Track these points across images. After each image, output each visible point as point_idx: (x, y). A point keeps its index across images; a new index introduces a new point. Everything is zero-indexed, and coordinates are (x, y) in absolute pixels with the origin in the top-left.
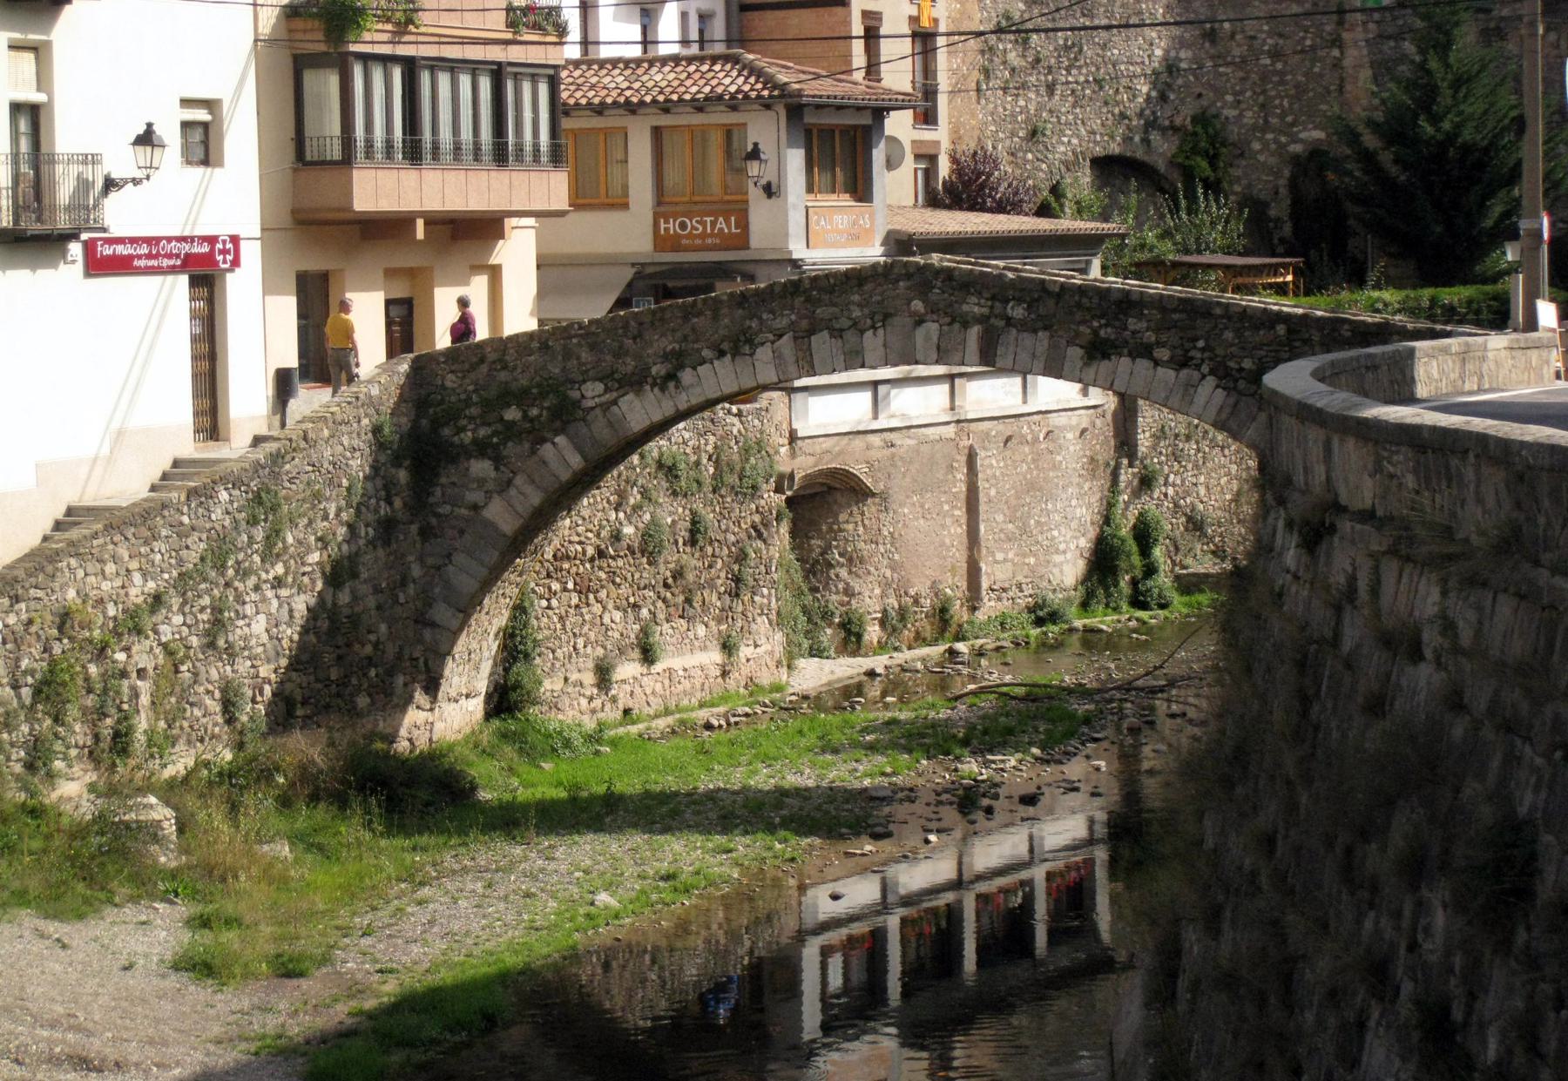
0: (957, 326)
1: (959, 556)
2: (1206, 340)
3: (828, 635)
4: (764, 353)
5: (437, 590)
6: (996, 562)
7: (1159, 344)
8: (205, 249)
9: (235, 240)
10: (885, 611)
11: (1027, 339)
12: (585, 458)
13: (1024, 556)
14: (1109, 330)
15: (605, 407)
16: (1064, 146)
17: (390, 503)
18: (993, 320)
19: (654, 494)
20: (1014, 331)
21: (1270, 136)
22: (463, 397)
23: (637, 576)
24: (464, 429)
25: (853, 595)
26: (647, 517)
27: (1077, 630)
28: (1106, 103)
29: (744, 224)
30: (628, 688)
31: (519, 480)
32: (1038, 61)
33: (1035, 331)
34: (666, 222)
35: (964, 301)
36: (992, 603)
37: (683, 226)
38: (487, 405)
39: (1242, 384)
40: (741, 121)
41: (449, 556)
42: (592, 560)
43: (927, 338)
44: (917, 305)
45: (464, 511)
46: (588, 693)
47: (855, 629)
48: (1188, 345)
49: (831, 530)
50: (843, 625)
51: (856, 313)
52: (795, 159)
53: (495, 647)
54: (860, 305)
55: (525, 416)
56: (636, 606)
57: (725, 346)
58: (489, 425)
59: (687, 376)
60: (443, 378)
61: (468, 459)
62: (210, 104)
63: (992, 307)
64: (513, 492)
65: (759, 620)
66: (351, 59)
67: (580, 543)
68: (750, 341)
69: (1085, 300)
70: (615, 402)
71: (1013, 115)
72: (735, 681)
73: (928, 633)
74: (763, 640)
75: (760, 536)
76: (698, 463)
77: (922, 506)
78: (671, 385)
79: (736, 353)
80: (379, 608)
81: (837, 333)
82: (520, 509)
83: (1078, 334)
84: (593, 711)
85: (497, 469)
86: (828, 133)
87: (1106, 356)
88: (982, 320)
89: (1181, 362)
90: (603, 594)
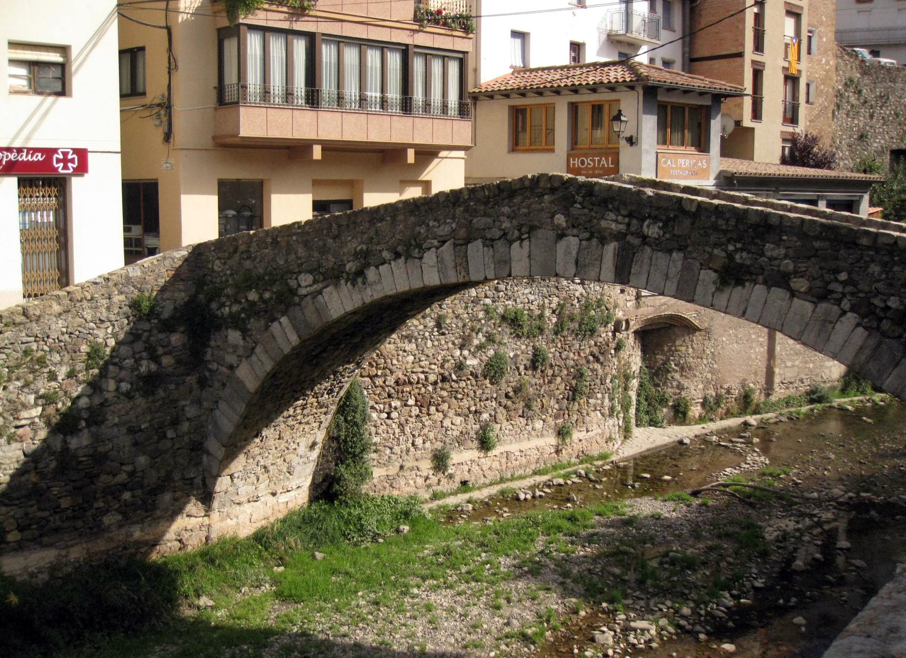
0: (594, 241)
1: (762, 366)
2: (849, 274)
4: (430, 258)
6: (787, 367)
7: (796, 273)
8: (39, 157)
9: (82, 154)
10: (705, 399)
11: (661, 259)
12: (299, 337)
13: (806, 362)
14: (744, 254)
16: (877, 143)
18: (629, 238)
19: (498, 338)
23: (479, 392)
25: (683, 389)
27: (834, 408)
28: (900, 124)
29: (616, 162)
30: (466, 468)
31: (258, 350)
32: (865, 102)
33: (670, 251)
34: (574, 160)
35: (603, 218)
36: (782, 391)
37: (583, 163)
40: (617, 98)
42: (435, 383)
43: (567, 252)
44: (560, 219)
45: (224, 369)
46: (425, 474)
47: (682, 409)
48: (827, 277)
49: (670, 350)
50: (674, 407)
51: (506, 224)
52: (649, 124)
55: (261, 298)
57: (400, 249)
59: (371, 273)
61: (227, 328)
62: (64, 50)
63: (628, 225)
64: (254, 358)
65: (592, 414)
66: (242, 27)
67: (423, 372)
68: (419, 246)
69: (721, 222)
70: (320, 292)
71: (851, 128)
73: (735, 410)
74: (595, 426)
75: (597, 360)
76: (541, 316)
77: (736, 336)
79: (409, 256)
81: (489, 243)
84: (429, 486)
85: (244, 339)
86: (679, 109)
87: (740, 282)
88: (619, 237)
89: (820, 295)
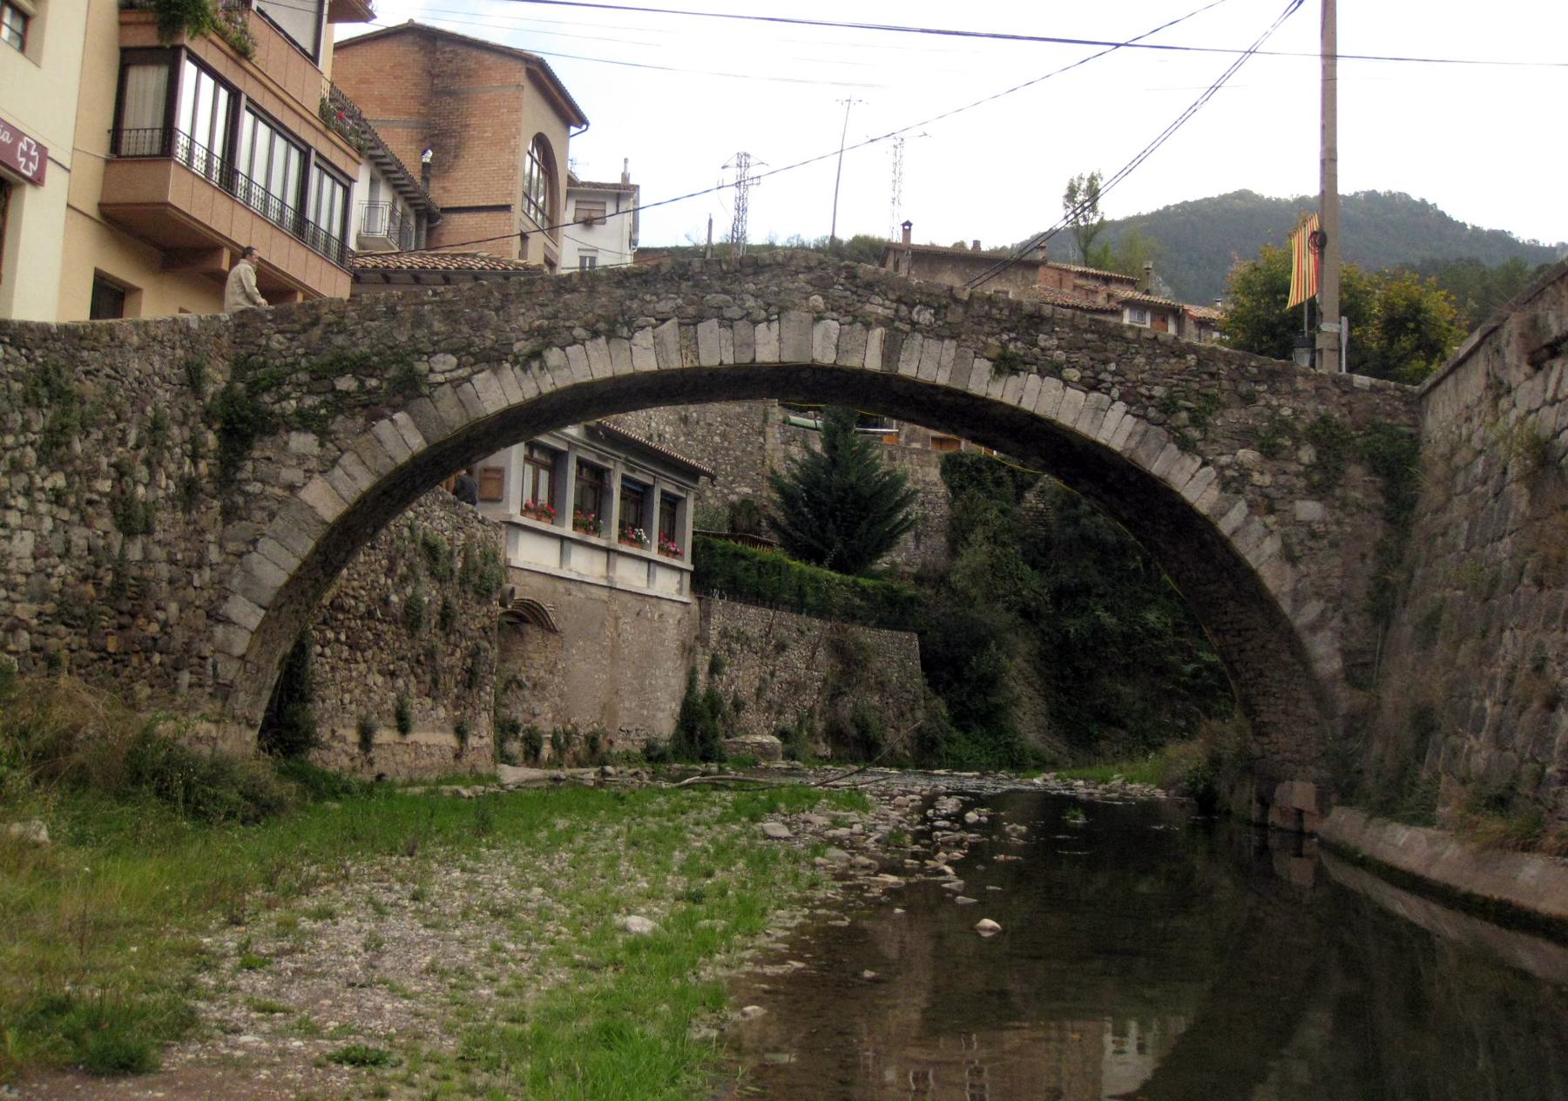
0: (858, 326)
3: (515, 747)
4: (644, 339)
5: (235, 582)
10: (555, 733)
11: (933, 346)
15: (456, 384)
17: (195, 463)
18: (897, 324)
20: (919, 336)
22: (290, 360)
24: (287, 397)
26: (409, 590)
31: (347, 459)
33: (941, 338)
39: (1152, 412)
41: (254, 542)
43: (826, 336)
44: (817, 300)
45: (278, 491)
48: (1099, 367)
54: (756, 296)
56: (393, 674)
57: (602, 326)
58: (318, 394)
59: (553, 356)
60: (269, 338)
61: (288, 432)
63: (897, 311)
64: (338, 472)
67: (354, 597)
70: (468, 379)
79: (611, 335)
80: (171, 582)
82: (345, 494)
83: (986, 346)
85: (321, 445)
87: (1015, 371)
88: (886, 322)
89: (1091, 385)
90: (369, 654)
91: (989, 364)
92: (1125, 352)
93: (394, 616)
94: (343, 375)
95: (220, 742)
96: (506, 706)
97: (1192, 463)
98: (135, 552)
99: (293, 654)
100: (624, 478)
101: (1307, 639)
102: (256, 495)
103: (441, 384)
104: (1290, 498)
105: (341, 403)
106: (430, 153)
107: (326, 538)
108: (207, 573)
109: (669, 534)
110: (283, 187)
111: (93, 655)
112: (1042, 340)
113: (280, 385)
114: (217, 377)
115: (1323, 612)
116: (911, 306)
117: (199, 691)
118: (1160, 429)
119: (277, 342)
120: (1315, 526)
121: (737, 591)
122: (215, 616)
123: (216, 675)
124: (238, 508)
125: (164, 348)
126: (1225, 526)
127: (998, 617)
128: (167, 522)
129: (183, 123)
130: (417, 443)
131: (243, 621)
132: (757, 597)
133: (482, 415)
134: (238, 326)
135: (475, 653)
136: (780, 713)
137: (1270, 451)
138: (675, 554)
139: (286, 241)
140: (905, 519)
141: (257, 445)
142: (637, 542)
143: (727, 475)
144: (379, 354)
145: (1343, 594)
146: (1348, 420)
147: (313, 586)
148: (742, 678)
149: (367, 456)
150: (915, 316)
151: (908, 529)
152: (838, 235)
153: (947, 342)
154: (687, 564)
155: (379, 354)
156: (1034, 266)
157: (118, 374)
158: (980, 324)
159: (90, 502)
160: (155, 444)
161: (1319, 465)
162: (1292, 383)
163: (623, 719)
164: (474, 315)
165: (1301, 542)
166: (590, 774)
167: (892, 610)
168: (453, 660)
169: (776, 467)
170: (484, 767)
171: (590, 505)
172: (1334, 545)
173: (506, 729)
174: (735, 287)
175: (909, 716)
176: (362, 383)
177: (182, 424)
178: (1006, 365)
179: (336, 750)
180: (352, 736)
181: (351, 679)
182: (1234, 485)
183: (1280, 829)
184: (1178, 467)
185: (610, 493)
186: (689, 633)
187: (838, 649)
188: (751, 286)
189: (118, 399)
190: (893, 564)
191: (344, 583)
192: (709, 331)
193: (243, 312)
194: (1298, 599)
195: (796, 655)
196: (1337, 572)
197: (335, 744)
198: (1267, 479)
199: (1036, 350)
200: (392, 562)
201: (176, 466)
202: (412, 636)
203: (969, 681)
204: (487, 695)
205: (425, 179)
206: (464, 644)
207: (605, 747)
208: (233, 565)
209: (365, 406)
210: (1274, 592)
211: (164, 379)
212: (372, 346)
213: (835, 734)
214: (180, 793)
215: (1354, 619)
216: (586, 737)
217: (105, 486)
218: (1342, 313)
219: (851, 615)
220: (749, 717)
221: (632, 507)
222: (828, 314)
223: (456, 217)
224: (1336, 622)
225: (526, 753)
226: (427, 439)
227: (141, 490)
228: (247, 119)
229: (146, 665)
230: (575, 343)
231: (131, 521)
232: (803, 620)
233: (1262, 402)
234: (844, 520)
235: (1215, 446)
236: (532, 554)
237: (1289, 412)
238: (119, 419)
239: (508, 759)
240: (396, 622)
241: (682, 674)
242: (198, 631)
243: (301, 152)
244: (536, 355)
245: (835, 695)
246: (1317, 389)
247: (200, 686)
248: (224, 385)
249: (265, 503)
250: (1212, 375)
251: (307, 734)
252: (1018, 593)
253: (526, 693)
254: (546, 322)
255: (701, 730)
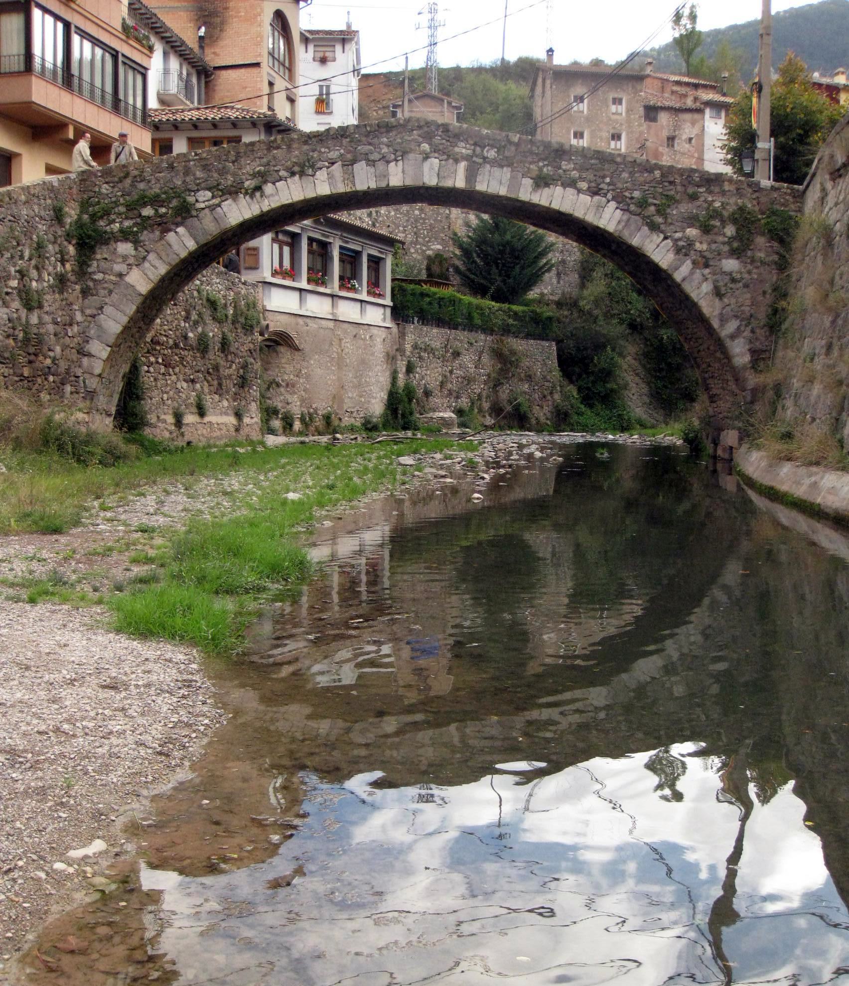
0: (451, 161)
3: (276, 424)
4: (322, 175)
5: (92, 332)
7: (582, 179)
10: (302, 414)
11: (497, 171)
14: (550, 168)
15: (212, 208)
17: (63, 265)
18: (474, 159)
20: (488, 166)
21: (418, 247)
22: (113, 199)
24: (114, 221)
31: (151, 257)
33: (502, 167)
35: (456, 146)
38: (130, 207)
43: (431, 168)
44: (426, 147)
45: (113, 278)
53: (121, 385)
54: (388, 146)
56: (193, 381)
57: (296, 169)
59: (268, 188)
60: (100, 187)
61: (116, 242)
63: (474, 151)
64: (147, 265)
70: (219, 205)
72: (242, 436)
78: (258, 194)
79: (302, 174)
81: (371, 163)
82: (152, 277)
85: (136, 249)
87: (547, 185)
88: (467, 158)
89: (595, 192)
90: (177, 370)
91: (532, 181)
92: (615, 171)
93: (191, 345)
94: (145, 207)
95: (91, 424)
96: (269, 398)
97: (657, 238)
98: (34, 320)
99: (130, 372)
100: (341, 247)
101: (728, 343)
102: (100, 281)
103: (203, 209)
104: (718, 258)
105: (145, 223)
106: (203, 29)
107: (144, 303)
108: (75, 328)
109: (375, 284)
110: (103, 80)
111: (17, 379)
112: (565, 165)
113: (109, 214)
114: (72, 213)
115: (738, 328)
116: (483, 147)
117: (77, 396)
118: (637, 218)
119: (105, 189)
120: (734, 275)
121: (425, 318)
122: (82, 353)
123: (85, 386)
124: (90, 289)
125: (39, 200)
126: (678, 276)
127: (614, 329)
128: (51, 301)
129: (37, 50)
130: (191, 245)
131: (98, 354)
132: (440, 322)
133: (228, 226)
134: (81, 180)
135: (245, 366)
136: (457, 397)
137: (706, 229)
138: (380, 296)
139: (107, 115)
140: (546, 264)
141: (98, 251)
142: (353, 289)
143: (424, 238)
144: (165, 193)
145: (751, 316)
146: (757, 208)
147: (138, 332)
148: (429, 375)
149: (163, 254)
150: (485, 154)
151: (549, 270)
152: (507, 58)
153: (505, 169)
154: (388, 301)
155: (165, 193)
156: (639, 78)
157: (16, 219)
158: (526, 157)
159: (7, 293)
160: (39, 257)
161: (738, 237)
162: (721, 186)
163: (348, 405)
164: (220, 166)
165: (726, 285)
166: (324, 439)
167: (538, 326)
168: (231, 371)
169: (457, 230)
170: (255, 436)
171: (319, 266)
172: (746, 286)
173: (269, 413)
174: (376, 141)
175: (549, 397)
176: (156, 210)
177: (54, 243)
178: (542, 182)
179: (160, 425)
180: (170, 419)
181: (167, 385)
182: (684, 251)
183: (722, 459)
184: (648, 240)
185: (332, 258)
186: (391, 347)
187: (499, 355)
188: (385, 140)
189: (17, 233)
190: (542, 294)
191: (159, 327)
192: (360, 168)
193: (83, 172)
194: (723, 320)
195: (468, 359)
196: (748, 302)
197: (160, 424)
198: (705, 247)
199: (561, 171)
200: (188, 313)
201: (53, 267)
202: (203, 358)
203: (593, 373)
204: (255, 392)
205: (201, 47)
206: (237, 361)
207: (336, 422)
208: (90, 322)
209: (160, 225)
210: (707, 316)
211: (41, 218)
212: (161, 189)
213: (496, 410)
214: (70, 450)
215: (758, 331)
216: (323, 416)
217: (14, 283)
218: (771, 136)
219: (506, 330)
220: (435, 400)
221: (348, 267)
222: (432, 155)
223: (224, 73)
224: (747, 333)
225: (284, 428)
226: (197, 242)
227: (34, 284)
228: (76, 39)
229: (46, 383)
230: (281, 180)
231: (30, 302)
232: (472, 336)
233: (702, 199)
234: (504, 265)
235: (672, 227)
236: (281, 302)
237: (720, 204)
238: (18, 244)
239: (272, 431)
240: (193, 349)
241: (388, 373)
242: (73, 361)
243: (113, 55)
244: (258, 188)
245: (496, 385)
246: (738, 189)
247: (77, 393)
248: (76, 217)
249: (106, 285)
250: (671, 183)
251: (142, 418)
252: (628, 312)
253: (282, 389)
254: (262, 168)
255: (401, 411)
